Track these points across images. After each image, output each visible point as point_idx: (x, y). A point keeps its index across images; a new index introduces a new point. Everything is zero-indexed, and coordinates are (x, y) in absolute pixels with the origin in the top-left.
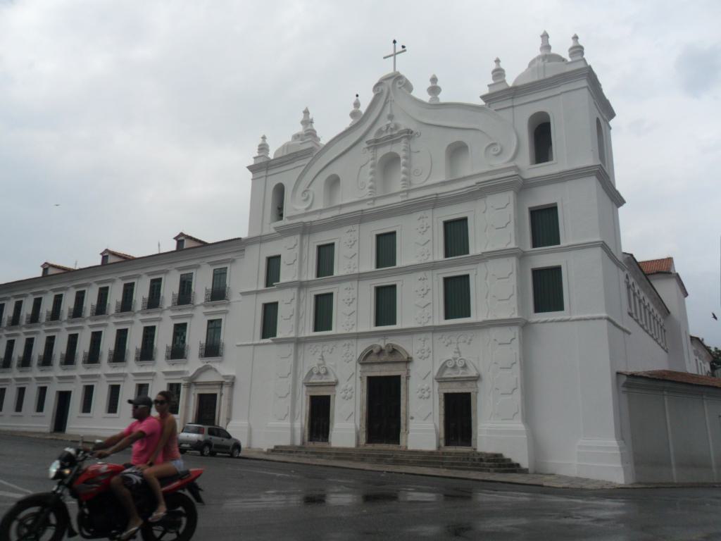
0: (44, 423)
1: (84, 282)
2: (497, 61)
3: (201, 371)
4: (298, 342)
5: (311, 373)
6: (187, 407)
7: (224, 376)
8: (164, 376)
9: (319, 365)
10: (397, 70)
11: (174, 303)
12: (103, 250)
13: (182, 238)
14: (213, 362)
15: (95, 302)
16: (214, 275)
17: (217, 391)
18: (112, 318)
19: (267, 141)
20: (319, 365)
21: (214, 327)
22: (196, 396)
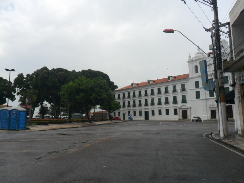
0: (143, 117)
1: (130, 90)
2: (190, 54)
3: (182, 106)
4: (206, 99)
5: (210, 105)
6: (180, 113)
7: (188, 107)
8: (138, 110)
9: (212, 104)
10: (224, 39)
11: (144, 96)
12: (148, 80)
13: (169, 77)
14: (185, 104)
15: (117, 97)
16: (182, 86)
17: (187, 110)
18: (163, 95)
19: (191, 55)
20: (212, 104)
21: (184, 97)
22: (182, 111)
